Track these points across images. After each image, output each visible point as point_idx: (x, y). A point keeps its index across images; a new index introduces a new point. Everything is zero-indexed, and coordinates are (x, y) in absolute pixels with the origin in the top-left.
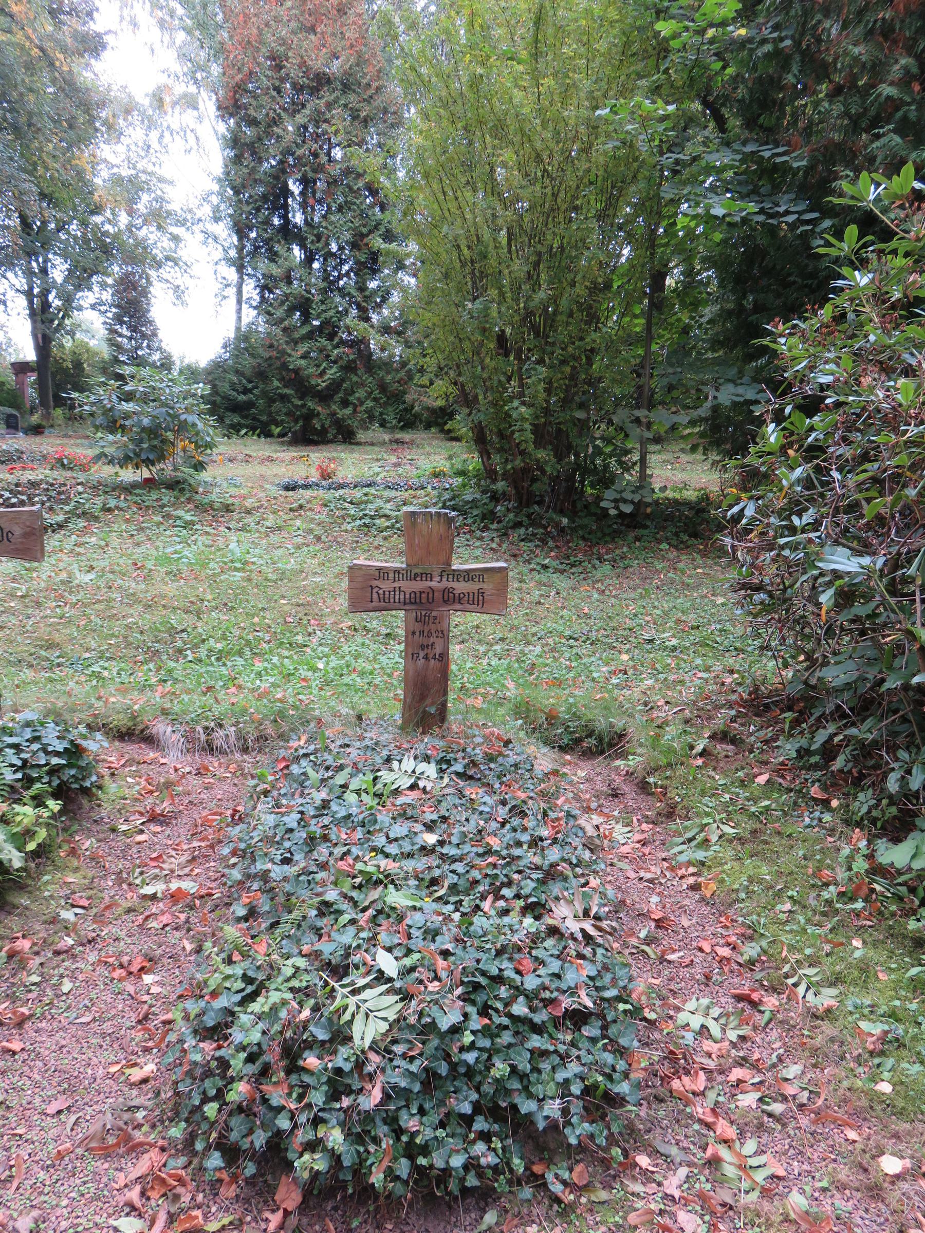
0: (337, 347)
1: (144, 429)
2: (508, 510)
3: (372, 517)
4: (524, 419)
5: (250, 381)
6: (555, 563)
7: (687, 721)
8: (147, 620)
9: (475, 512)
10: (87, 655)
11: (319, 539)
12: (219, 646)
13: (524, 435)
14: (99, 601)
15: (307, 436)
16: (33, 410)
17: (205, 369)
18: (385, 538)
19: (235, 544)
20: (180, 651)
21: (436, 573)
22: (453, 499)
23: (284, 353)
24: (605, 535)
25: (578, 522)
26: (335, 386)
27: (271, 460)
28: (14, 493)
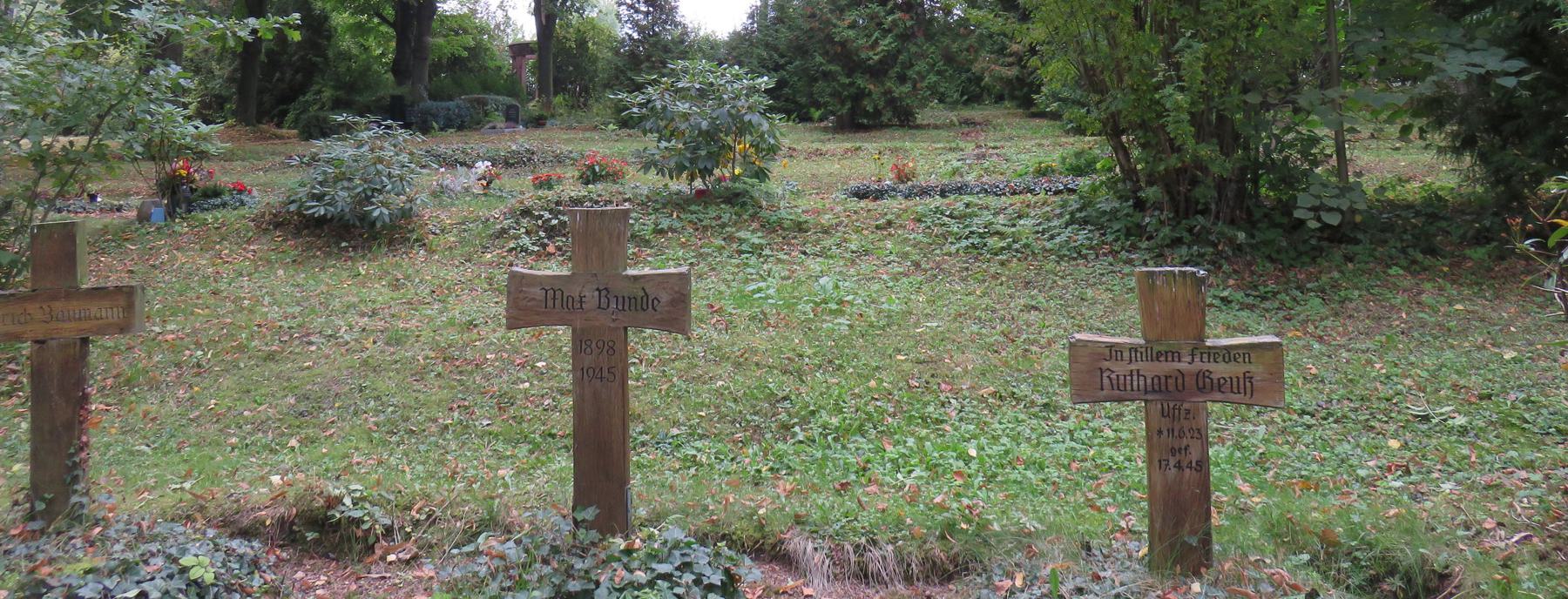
0: (891, 12)
1: (701, 132)
2: (1162, 222)
3: (981, 236)
4: (1178, 108)
5: (782, 56)
6: (1239, 295)
7: (1543, 557)
8: (741, 383)
9: (1116, 226)
10: (675, 431)
11: (917, 265)
12: (835, 421)
13: (1180, 129)
14: (678, 358)
15: (857, 119)
16: (531, 95)
17: (726, 43)
18: (1002, 264)
19: (827, 277)
20: (786, 427)
21: (1185, 351)
22: (1080, 210)
23: (828, 22)
24: (1300, 254)
25: (1259, 237)
26: (889, 59)
27: (819, 153)
28: (555, 213)
